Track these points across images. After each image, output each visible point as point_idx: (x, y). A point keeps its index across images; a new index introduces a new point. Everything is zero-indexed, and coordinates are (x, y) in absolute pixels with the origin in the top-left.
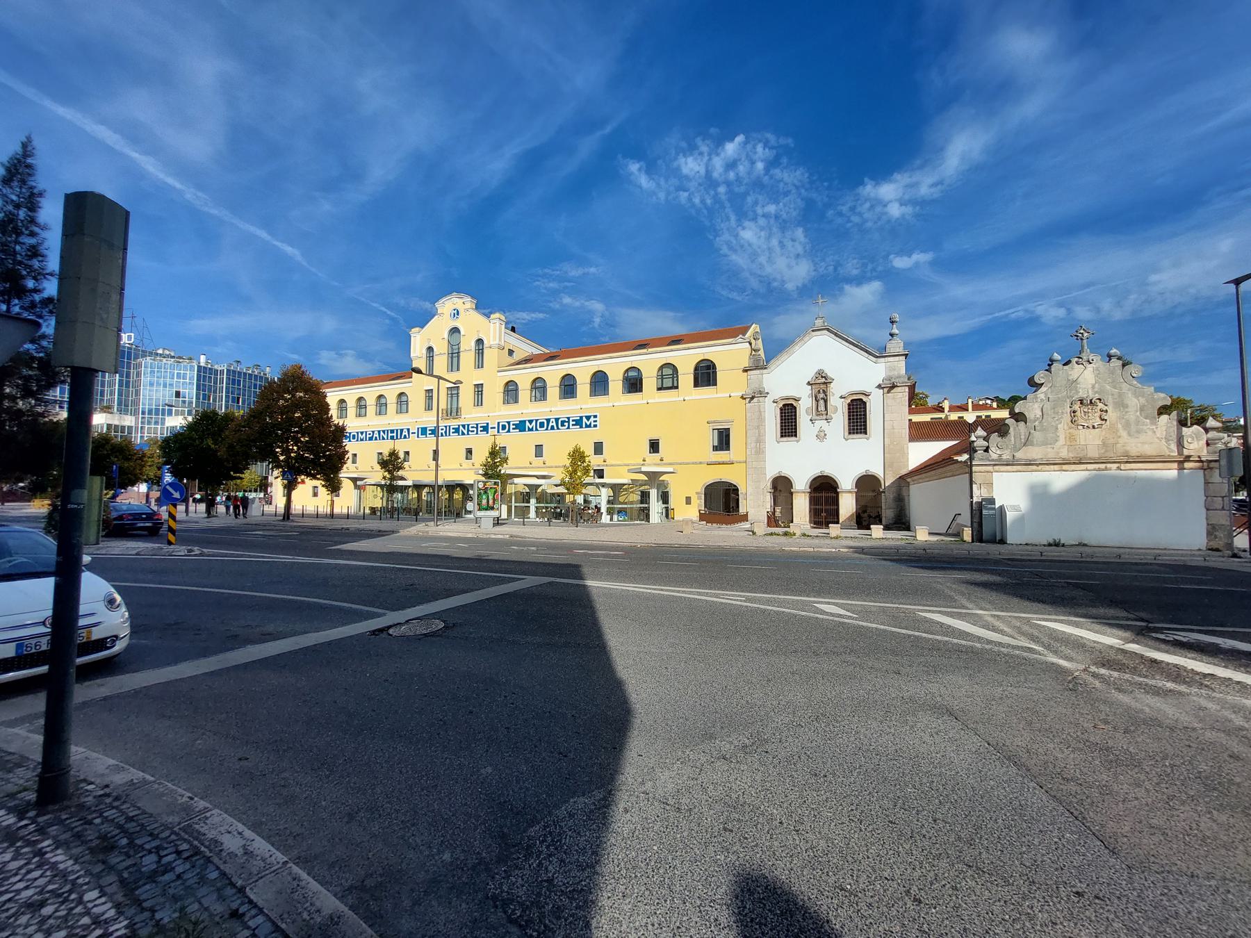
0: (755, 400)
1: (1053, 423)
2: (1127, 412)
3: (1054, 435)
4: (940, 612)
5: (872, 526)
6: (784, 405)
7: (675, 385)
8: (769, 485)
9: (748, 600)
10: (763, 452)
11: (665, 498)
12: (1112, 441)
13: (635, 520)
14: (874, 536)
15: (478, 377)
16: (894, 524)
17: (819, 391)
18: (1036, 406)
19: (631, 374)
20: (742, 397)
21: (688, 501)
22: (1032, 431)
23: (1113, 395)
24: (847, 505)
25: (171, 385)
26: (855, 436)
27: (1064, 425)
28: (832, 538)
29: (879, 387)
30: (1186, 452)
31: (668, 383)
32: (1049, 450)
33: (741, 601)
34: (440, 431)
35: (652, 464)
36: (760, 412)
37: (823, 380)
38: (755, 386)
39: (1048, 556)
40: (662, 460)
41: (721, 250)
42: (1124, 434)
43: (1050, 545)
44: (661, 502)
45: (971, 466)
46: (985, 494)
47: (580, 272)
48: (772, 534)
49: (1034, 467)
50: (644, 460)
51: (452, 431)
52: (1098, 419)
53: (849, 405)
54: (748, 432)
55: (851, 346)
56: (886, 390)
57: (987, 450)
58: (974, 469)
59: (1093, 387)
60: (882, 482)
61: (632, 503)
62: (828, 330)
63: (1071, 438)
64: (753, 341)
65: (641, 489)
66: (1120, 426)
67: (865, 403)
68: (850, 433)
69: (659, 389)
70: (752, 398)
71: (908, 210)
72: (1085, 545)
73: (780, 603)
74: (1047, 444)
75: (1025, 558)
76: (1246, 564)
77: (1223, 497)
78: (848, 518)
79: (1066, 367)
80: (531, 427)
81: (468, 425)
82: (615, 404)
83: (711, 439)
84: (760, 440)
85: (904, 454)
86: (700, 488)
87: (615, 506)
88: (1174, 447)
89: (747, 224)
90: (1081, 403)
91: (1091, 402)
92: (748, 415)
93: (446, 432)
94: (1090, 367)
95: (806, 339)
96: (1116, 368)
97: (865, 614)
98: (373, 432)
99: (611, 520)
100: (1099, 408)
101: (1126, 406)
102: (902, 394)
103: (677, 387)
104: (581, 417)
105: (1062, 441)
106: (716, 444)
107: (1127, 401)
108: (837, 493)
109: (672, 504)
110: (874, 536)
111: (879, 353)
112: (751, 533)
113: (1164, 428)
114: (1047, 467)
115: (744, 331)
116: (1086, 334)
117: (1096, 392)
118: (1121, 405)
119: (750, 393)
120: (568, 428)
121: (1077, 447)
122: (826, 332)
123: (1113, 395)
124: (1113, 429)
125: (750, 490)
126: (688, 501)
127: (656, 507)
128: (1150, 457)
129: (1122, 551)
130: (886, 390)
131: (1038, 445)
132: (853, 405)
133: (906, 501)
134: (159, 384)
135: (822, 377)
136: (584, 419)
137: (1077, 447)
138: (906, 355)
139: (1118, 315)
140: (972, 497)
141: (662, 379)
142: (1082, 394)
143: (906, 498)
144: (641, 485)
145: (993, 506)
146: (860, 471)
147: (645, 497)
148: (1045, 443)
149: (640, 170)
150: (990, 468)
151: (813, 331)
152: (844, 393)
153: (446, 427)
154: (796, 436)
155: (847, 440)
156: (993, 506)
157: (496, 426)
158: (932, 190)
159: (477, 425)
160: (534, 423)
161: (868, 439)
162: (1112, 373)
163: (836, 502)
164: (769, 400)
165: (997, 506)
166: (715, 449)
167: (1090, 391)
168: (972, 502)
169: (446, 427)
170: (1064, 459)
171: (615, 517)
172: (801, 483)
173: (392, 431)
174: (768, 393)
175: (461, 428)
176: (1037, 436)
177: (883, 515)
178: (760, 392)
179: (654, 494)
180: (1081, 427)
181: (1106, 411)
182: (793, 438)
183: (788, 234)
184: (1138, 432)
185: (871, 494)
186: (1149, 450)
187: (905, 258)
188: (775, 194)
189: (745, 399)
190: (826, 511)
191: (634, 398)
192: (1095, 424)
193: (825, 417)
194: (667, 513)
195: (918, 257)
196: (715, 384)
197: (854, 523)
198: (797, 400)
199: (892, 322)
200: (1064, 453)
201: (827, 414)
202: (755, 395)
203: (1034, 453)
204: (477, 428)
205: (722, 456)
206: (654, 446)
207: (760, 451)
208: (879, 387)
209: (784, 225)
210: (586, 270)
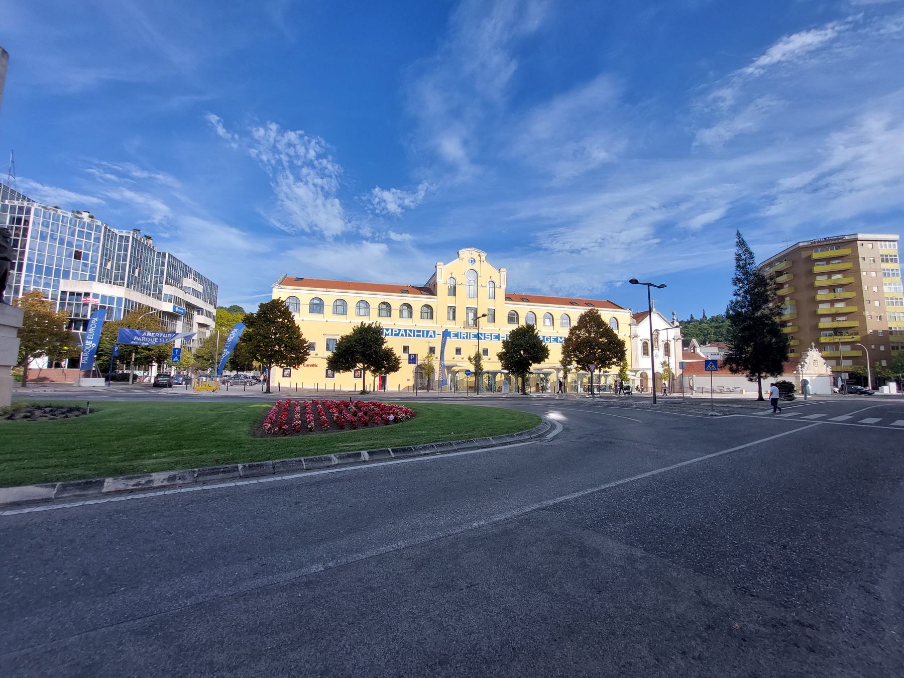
15: (451, 301)
25: (70, 244)
34: (462, 336)
47: (145, 174)
51: (471, 336)
71: (399, 210)
80: (387, 333)
81: (485, 334)
84: (637, 356)
89: (301, 184)
93: (467, 337)
98: (400, 330)
104: (557, 337)
120: (550, 342)
134: (53, 238)
136: (559, 339)
149: (219, 121)
153: (467, 333)
158: (411, 204)
159: (491, 334)
160: (390, 331)
164: (639, 338)
169: (467, 333)
173: (419, 331)
183: (329, 200)
187: (398, 235)
188: (322, 174)
195: (407, 237)
204: (491, 336)
209: (327, 195)
210: (153, 175)
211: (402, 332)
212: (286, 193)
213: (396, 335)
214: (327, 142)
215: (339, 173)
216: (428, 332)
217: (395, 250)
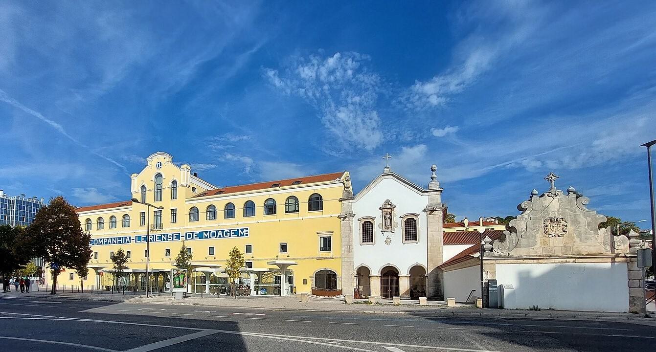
0: (347, 219)
2: (579, 226)
5: (420, 298)
8: (356, 271)
9: (342, 344)
11: (290, 280)
14: (421, 304)
15: (173, 204)
19: (269, 202)
20: (339, 217)
21: (305, 282)
22: (520, 238)
24: (404, 285)
27: (540, 235)
28: (395, 305)
29: (424, 210)
31: (292, 208)
34: (150, 238)
38: (347, 210)
42: (578, 240)
43: (531, 309)
46: (491, 278)
47: (237, 139)
48: (357, 303)
49: (521, 261)
51: (157, 238)
57: (492, 250)
59: (558, 211)
61: (269, 283)
62: (392, 175)
63: (545, 243)
64: (345, 182)
69: (286, 212)
70: (345, 218)
72: (553, 310)
74: (529, 246)
77: (639, 280)
80: (242, 233)
84: (350, 244)
85: (440, 253)
86: (312, 274)
87: (259, 285)
88: (609, 248)
89: (342, 109)
90: (551, 221)
98: (108, 239)
99: (257, 294)
103: (298, 211)
105: (539, 244)
108: (398, 277)
110: (421, 304)
113: (603, 237)
115: (340, 176)
117: (560, 214)
118: (576, 222)
124: (571, 237)
126: (305, 282)
127: (285, 286)
136: (240, 231)
138: (441, 191)
140: (482, 280)
142: (551, 215)
144: (276, 272)
146: (412, 263)
147: (278, 280)
148: (528, 246)
149: (274, 75)
152: (402, 215)
153: (153, 236)
154: (372, 241)
155: (404, 244)
157: (135, 239)
158: (458, 87)
160: (102, 241)
161: (373, 245)
162: (570, 202)
164: (355, 219)
166: (322, 249)
167: (556, 213)
168: (482, 283)
169: (153, 236)
171: (259, 292)
172: (375, 271)
174: (355, 215)
175: (163, 236)
179: (283, 277)
182: (371, 243)
183: (367, 115)
184: (587, 239)
186: (593, 250)
191: (271, 218)
195: (448, 129)
198: (373, 219)
200: (540, 252)
201: (392, 228)
204: (173, 236)
205: (326, 254)
206: (284, 248)
207: (350, 251)
208: (424, 210)
211: (220, 233)
212: (330, 121)
213: (106, 243)
214: (361, 54)
215: (375, 82)
216: (217, 232)
217: (435, 146)
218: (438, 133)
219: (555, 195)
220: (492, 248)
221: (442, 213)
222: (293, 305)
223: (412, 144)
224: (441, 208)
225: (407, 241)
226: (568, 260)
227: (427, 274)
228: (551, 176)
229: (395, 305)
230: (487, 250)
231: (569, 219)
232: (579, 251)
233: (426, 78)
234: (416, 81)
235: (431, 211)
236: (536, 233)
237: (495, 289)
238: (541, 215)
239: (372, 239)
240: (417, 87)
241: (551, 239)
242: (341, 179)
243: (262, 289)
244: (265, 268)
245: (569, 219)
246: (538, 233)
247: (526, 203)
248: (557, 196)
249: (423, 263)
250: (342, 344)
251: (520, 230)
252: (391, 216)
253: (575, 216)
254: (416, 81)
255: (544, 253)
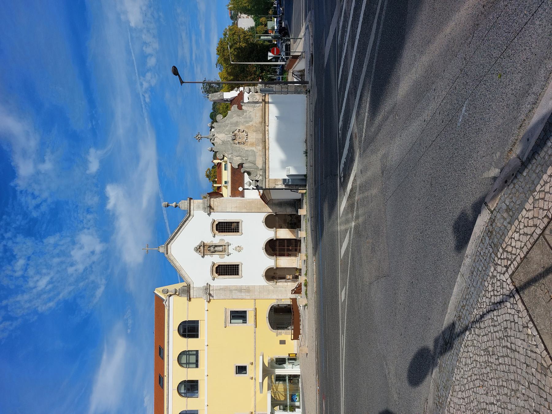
0: (211, 292)
1: (244, 152)
2: (240, 122)
3: (250, 152)
4: (341, 249)
6: (217, 273)
7: (195, 353)
8: (271, 283)
9: (343, 333)
10: (248, 287)
11: (281, 362)
12: (254, 129)
13: (298, 387)
14: (305, 236)
16: (295, 208)
17: (209, 250)
18: (235, 158)
19: (183, 391)
20: (209, 302)
21: (283, 342)
22: (248, 161)
23: (231, 127)
24: (284, 234)
26: (240, 228)
27: (246, 148)
28: (307, 259)
29: (209, 214)
30: (261, 100)
31: (193, 359)
32: (258, 154)
33: (343, 338)
35: (258, 372)
36: (220, 289)
37: (202, 248)
38: (201, 293)
39: (313, 164)
40: (252, 364)
41: (60, 299)
42: (251, 124)
43: (307, 156)
44: (285, 365)
45: (266, 189)
46: (281, 182)
48: (306, 294)
49: (267, 161)
50: (252, 378)
52: (243, 133)
53: (219, 232)
54: (234, 297)
55: (181, 231)
56: (212, 211)
57: (257, 181)
58: (267, 187)
59: (227, 134)
60: (271, 213)
61: (285, 390)
62: (168, 244)
63: (252, 144)
64: (169, 294)
65: (274, 382)
66: (247, 125)
67: (219, 223)
68: (238, 232)
69: (197, 366)
70: (210, 295)
72: (306, 140)
73: (343, 319)
74: (255, 155)
75: (314, 173)
76: (313, 90)
77: (282, 88)
78: (293, 233)
79: (216, 145)
82: (206, 404)
83: (238, 325)
84: (240, 290)
85: (252, 202)
86: (273, 333)
87: (288, 404)
88: (258, 105)
90: (235, 140)
91: (234, 136)
92: (222, 297)
94: (216, 135)
95: (172, 258)
96: (218, 125)
97: (344, 284)
99: (298, 407)
100: (237, 133)
101: (237, 122)
102: (215, 202)
103: (197, 351)
105: (254, 149)
106: (241, 321)
107: (235, 121)
108: (277, 239)
109: (286, 356)
110: (305, 236)
111: (188, 214)
112: (306, 307)
113: (249, 108)
114: (267, 155)
116: (199, 136)
117: (229, 133)
118: (237, 124)
119: (205, 297)
121: (257, 142)
122: (169, 246)
123: (231, 127)
124: (248, 128)
125: (275, 297)
126: (283, 342)
127: (288, 370)
128: (262, 114)
129: (308, 164)
130: (212, 211)
131: (255, 159)
132: (220, 229)
133: (281, 201)
135: (200, 248)
137: (257, 142)
138: (191, 199)
139: (156, 46)
140: (282, 189)
141: (189, 363)
142: (230, 139)
143: (279, 201)
144: (272, 381)
145: (287, 180)
147: (280, 378)
148: (255, 156)
150: (267, 180)
151: (167, 254)
152: (212, 235)
154: (238, 265)
155: (242, 234)
156: (287, 180)
161: (242, 221)
162: (220, 126)
163: (282, 241)
164: (212, 283)
165: (287, 178)
166: (245, 321)
167: (229, 136)
168: (285, 189)
170: (263, 148)
171: (297, 404)
172: (270, 262)
174: (207, 284)
176: (251, 159)
177: (290, 213)
178: (206, 289)
179: (279, 371)
180: (247, 140)
181: (239, 130)
182: (240, 267)
184: (250, 118)
185: (277, 218)
186: (259, 114)
189: (210, 300)
190: (288, 246)
191: (202, 387)
192: (246, 135)
193: (227, 247)
194: (293, 359)
196: (197, 322)
197: (295, 230)
198: (214, 264)
199: (168, 206)
200: (260, 148)
201: (225, 245)
202: (208, 292)
203: (260, 164)
205: (250, 317)
206: (241, 370)
207: (248, 290)
208: (209, 214)
218: (94, 167)
219: (213, 136)
220: (256, 181)
221: (213, 199)
222: (312, 361)
223: (104, 199)
224: (208, 200)
225: (240, 230)
226: (266, 130)
227: (273, 213)
228: (197, 137)
229: (307, 259)
230: (257, 184)
231: (233, 128)
232: (260, 123)
233: (12, 173)
234: (12, 184)
235: (210, 209)
236: (244, 150)
237: (290, 181)
238: (229, 146)
239: (235, 265)
240: (21, 184)
241: (249, 140)
242: (164, 298)
243: (292, 400)
244: (268, 396)
245: (233, 128)
246: (244, 149)
247: (219, 155)
248: (214, 135)
249: (262, 216)
250: (343, 333)
251: (295, 297)
252: (212, 246)
253: (231, 124)
254: (12, 184)
255: (261, 145)
